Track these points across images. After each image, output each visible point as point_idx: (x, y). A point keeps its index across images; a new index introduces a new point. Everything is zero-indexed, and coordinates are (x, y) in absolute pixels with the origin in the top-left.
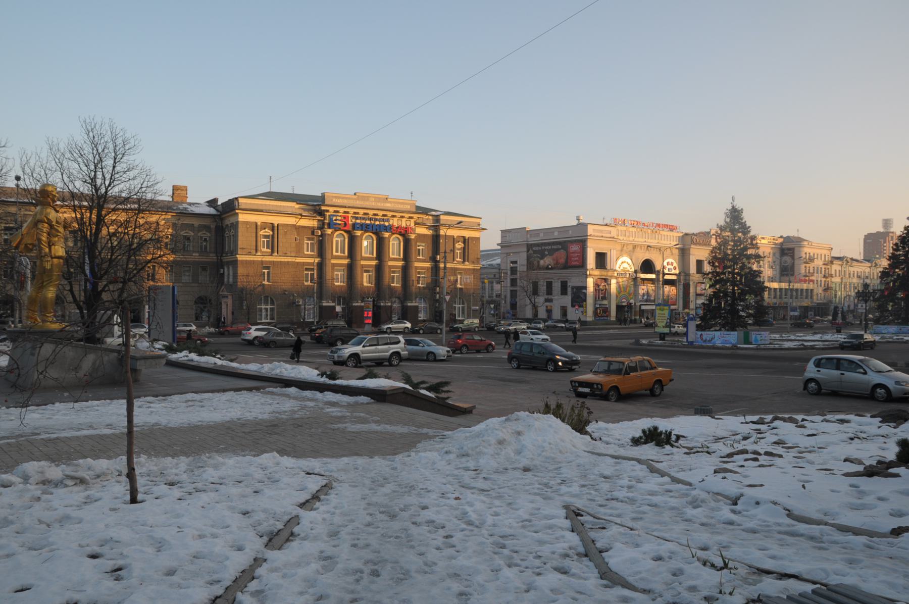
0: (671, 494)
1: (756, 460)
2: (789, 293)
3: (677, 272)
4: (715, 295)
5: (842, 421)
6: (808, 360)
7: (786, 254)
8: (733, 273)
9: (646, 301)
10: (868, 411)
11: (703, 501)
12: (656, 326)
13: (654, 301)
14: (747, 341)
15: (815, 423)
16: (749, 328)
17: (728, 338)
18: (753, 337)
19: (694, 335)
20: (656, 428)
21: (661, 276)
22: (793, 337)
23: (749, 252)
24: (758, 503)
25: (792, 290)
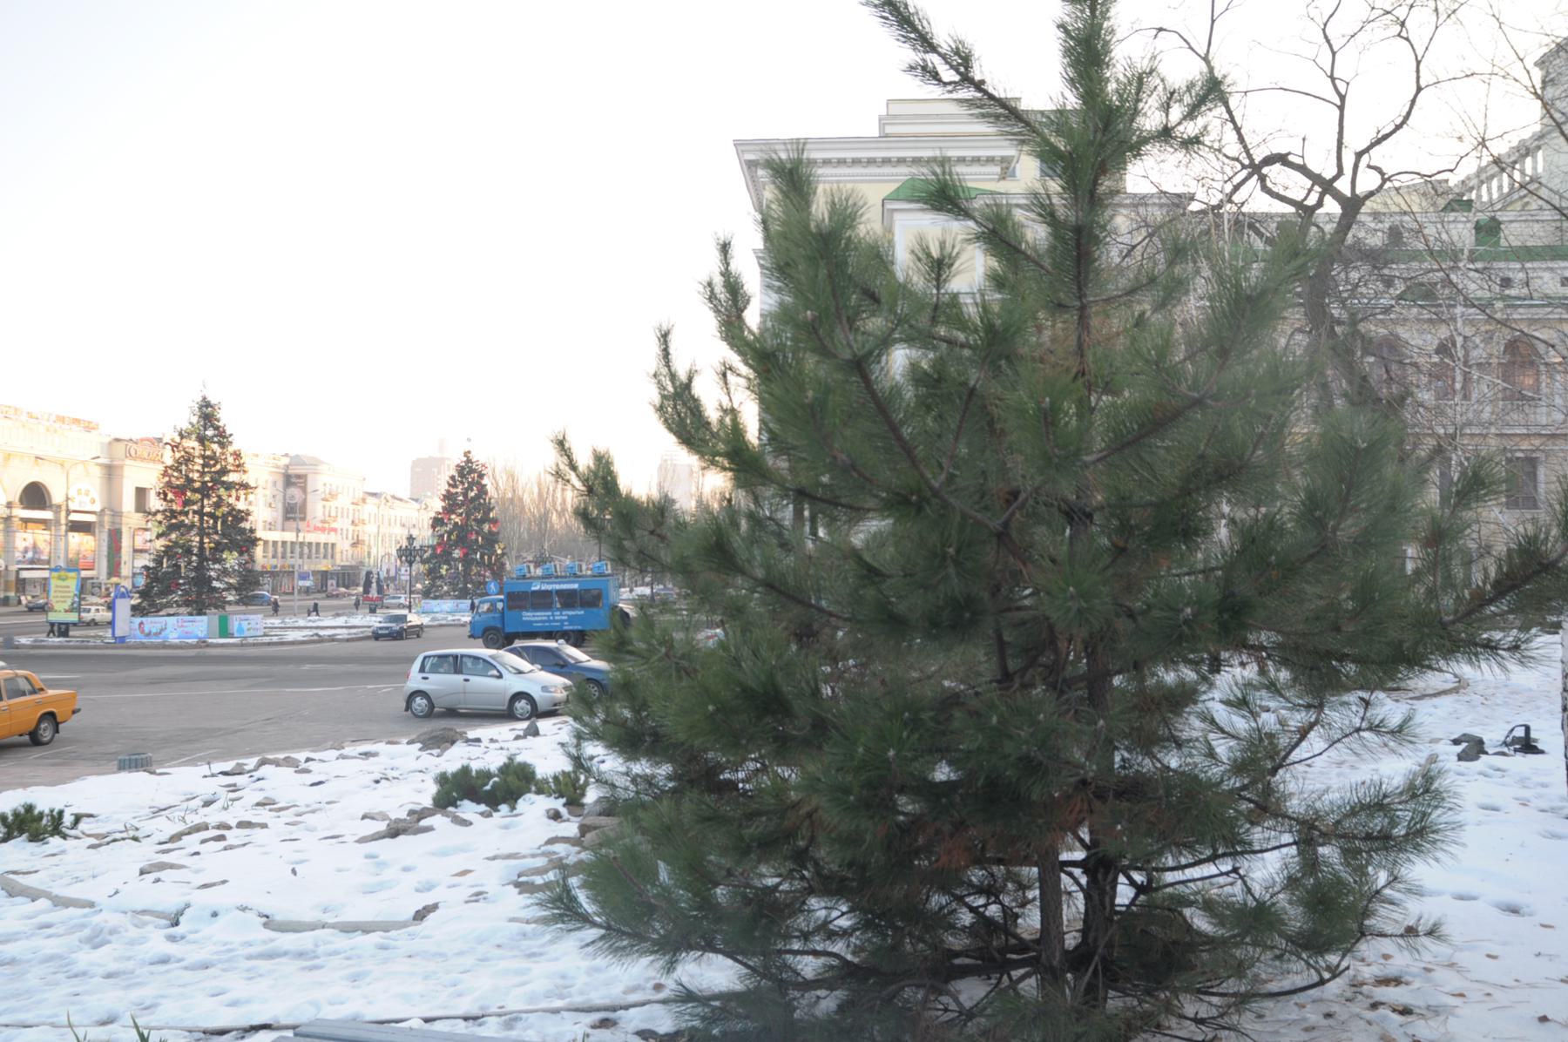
0: (49, 931)
1: (221, 838)
2: (298, 549)
3: (97, 508)
4: (168, 551)
5: (367, 755)
6: (412, 660)
7: (294, 484)
8: (200, 513)
9: (32, 562)
10: (403, 735)
11: (113, 932)
12: (52, 609)
13: (48, 562)
14: (224, 632)
15: (327, 763)
16: (228, 608)
17: (191, 627)
18: (236, 624)
19: (126, 623)
20: (29, 808)
21: (63, 514)
22: (302, 623)
23: (232, 477)
24: (215, 915)
25: (302, 544)
